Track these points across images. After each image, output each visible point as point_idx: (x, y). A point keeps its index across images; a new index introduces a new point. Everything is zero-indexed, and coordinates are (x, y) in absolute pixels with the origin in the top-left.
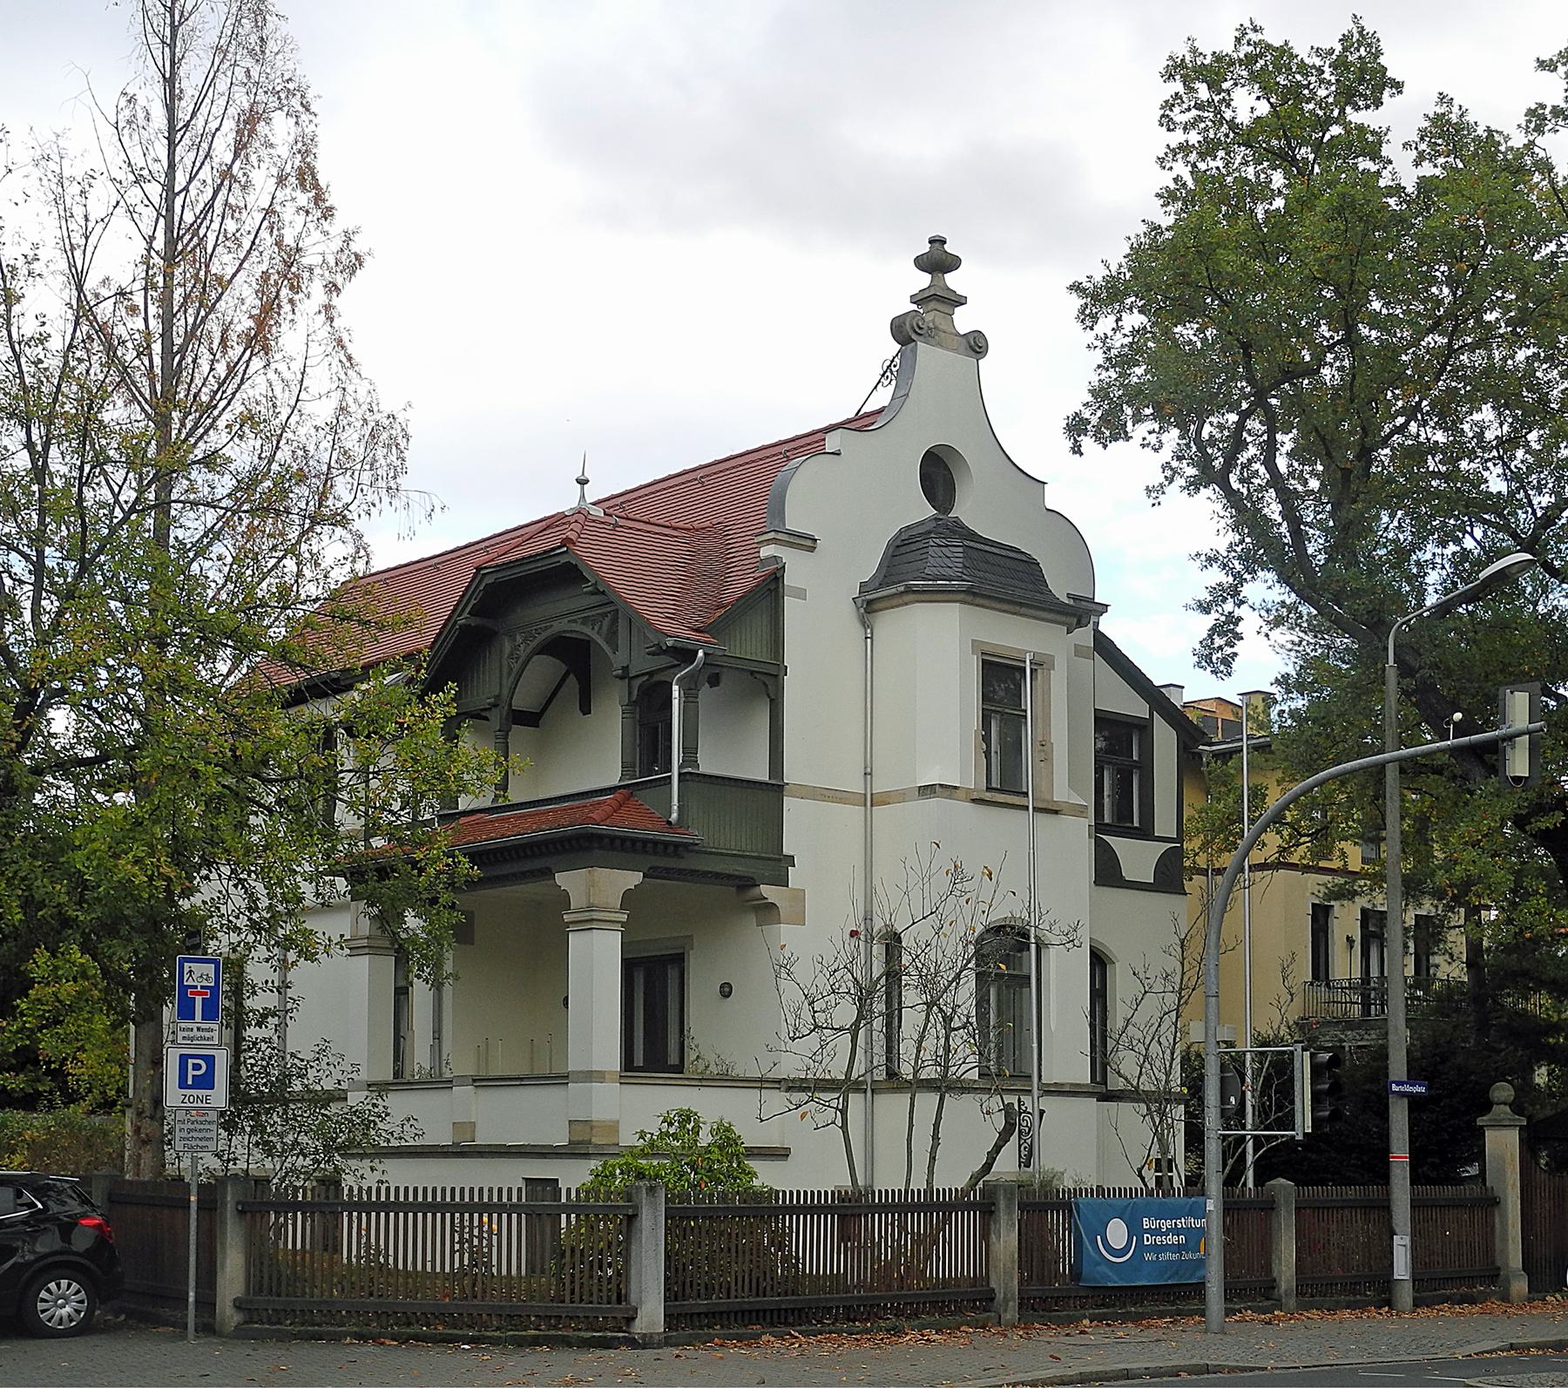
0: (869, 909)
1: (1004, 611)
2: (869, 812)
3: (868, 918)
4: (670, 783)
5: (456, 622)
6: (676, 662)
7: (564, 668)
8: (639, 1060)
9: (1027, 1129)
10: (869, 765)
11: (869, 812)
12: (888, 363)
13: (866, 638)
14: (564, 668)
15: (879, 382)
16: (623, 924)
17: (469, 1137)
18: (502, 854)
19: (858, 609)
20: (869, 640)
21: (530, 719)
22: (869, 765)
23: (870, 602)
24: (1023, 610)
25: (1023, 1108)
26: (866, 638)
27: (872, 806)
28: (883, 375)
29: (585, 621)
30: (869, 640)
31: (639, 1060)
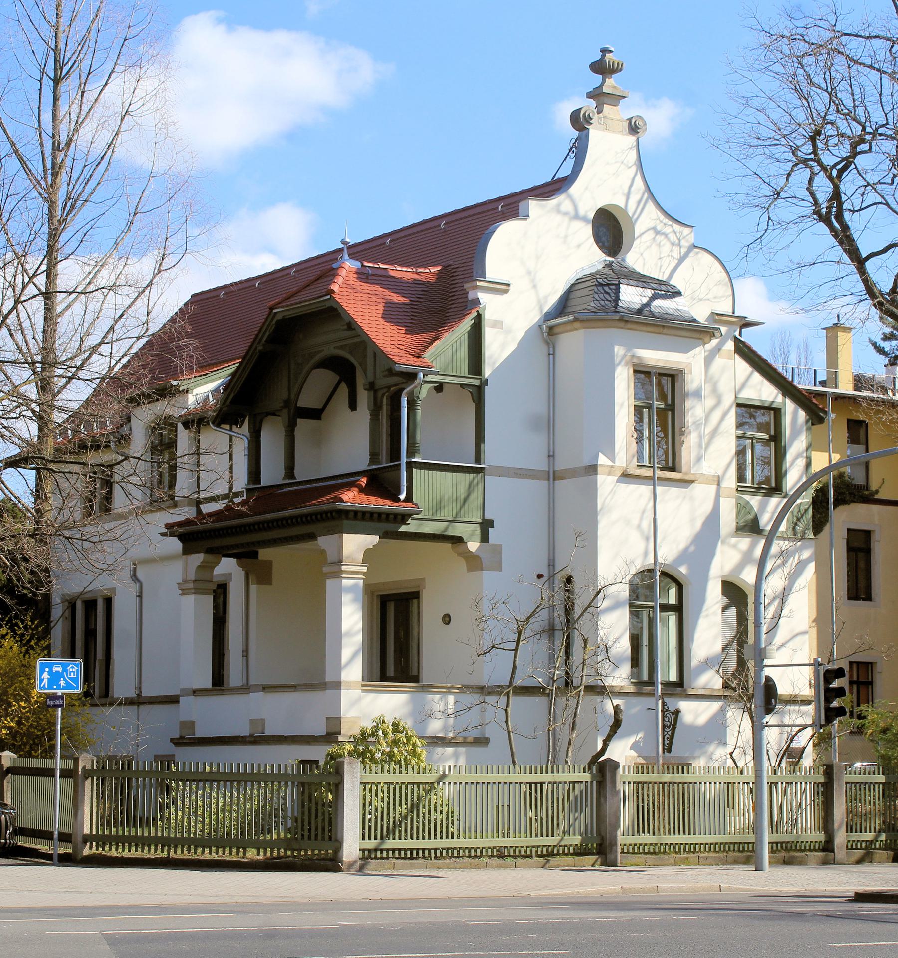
0: (551, 557)
1: (648, 332)
2: (552, 485)
3: (551, 564)
4: (400, 469)
5: (256, 348)
6: (404, 381)
7: (338, 378)
8: (391, 672)
9: (668, 723)
10: (552, 450)
11: (552, 485)
12: (573, 141)
13: (549, 354)
14: (338, 378)
15: (568, 155)
16: (364, 574)
17: (260, 729)
18: (263, 525)
19: (543, 333)
20: (551, 356)
21: (315, 414)
22: (552, 450)
23: (551, 328)
24: (665, 331)
25: (666, 707)
26: (549, 354)
27: (554, 479)
28: (570, 150)
29: (341, 347)
30: (551, 356)
31: (391, 672)
